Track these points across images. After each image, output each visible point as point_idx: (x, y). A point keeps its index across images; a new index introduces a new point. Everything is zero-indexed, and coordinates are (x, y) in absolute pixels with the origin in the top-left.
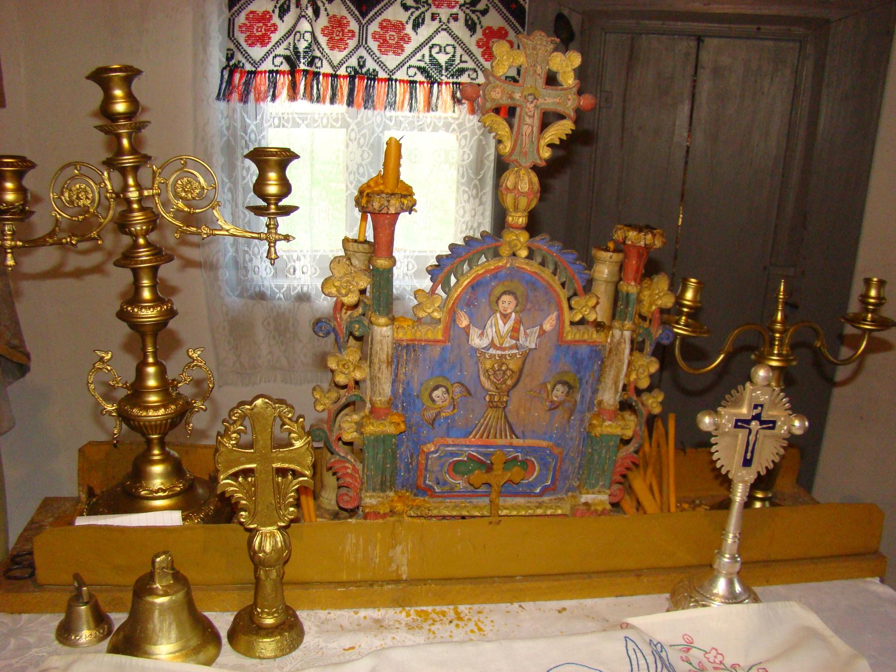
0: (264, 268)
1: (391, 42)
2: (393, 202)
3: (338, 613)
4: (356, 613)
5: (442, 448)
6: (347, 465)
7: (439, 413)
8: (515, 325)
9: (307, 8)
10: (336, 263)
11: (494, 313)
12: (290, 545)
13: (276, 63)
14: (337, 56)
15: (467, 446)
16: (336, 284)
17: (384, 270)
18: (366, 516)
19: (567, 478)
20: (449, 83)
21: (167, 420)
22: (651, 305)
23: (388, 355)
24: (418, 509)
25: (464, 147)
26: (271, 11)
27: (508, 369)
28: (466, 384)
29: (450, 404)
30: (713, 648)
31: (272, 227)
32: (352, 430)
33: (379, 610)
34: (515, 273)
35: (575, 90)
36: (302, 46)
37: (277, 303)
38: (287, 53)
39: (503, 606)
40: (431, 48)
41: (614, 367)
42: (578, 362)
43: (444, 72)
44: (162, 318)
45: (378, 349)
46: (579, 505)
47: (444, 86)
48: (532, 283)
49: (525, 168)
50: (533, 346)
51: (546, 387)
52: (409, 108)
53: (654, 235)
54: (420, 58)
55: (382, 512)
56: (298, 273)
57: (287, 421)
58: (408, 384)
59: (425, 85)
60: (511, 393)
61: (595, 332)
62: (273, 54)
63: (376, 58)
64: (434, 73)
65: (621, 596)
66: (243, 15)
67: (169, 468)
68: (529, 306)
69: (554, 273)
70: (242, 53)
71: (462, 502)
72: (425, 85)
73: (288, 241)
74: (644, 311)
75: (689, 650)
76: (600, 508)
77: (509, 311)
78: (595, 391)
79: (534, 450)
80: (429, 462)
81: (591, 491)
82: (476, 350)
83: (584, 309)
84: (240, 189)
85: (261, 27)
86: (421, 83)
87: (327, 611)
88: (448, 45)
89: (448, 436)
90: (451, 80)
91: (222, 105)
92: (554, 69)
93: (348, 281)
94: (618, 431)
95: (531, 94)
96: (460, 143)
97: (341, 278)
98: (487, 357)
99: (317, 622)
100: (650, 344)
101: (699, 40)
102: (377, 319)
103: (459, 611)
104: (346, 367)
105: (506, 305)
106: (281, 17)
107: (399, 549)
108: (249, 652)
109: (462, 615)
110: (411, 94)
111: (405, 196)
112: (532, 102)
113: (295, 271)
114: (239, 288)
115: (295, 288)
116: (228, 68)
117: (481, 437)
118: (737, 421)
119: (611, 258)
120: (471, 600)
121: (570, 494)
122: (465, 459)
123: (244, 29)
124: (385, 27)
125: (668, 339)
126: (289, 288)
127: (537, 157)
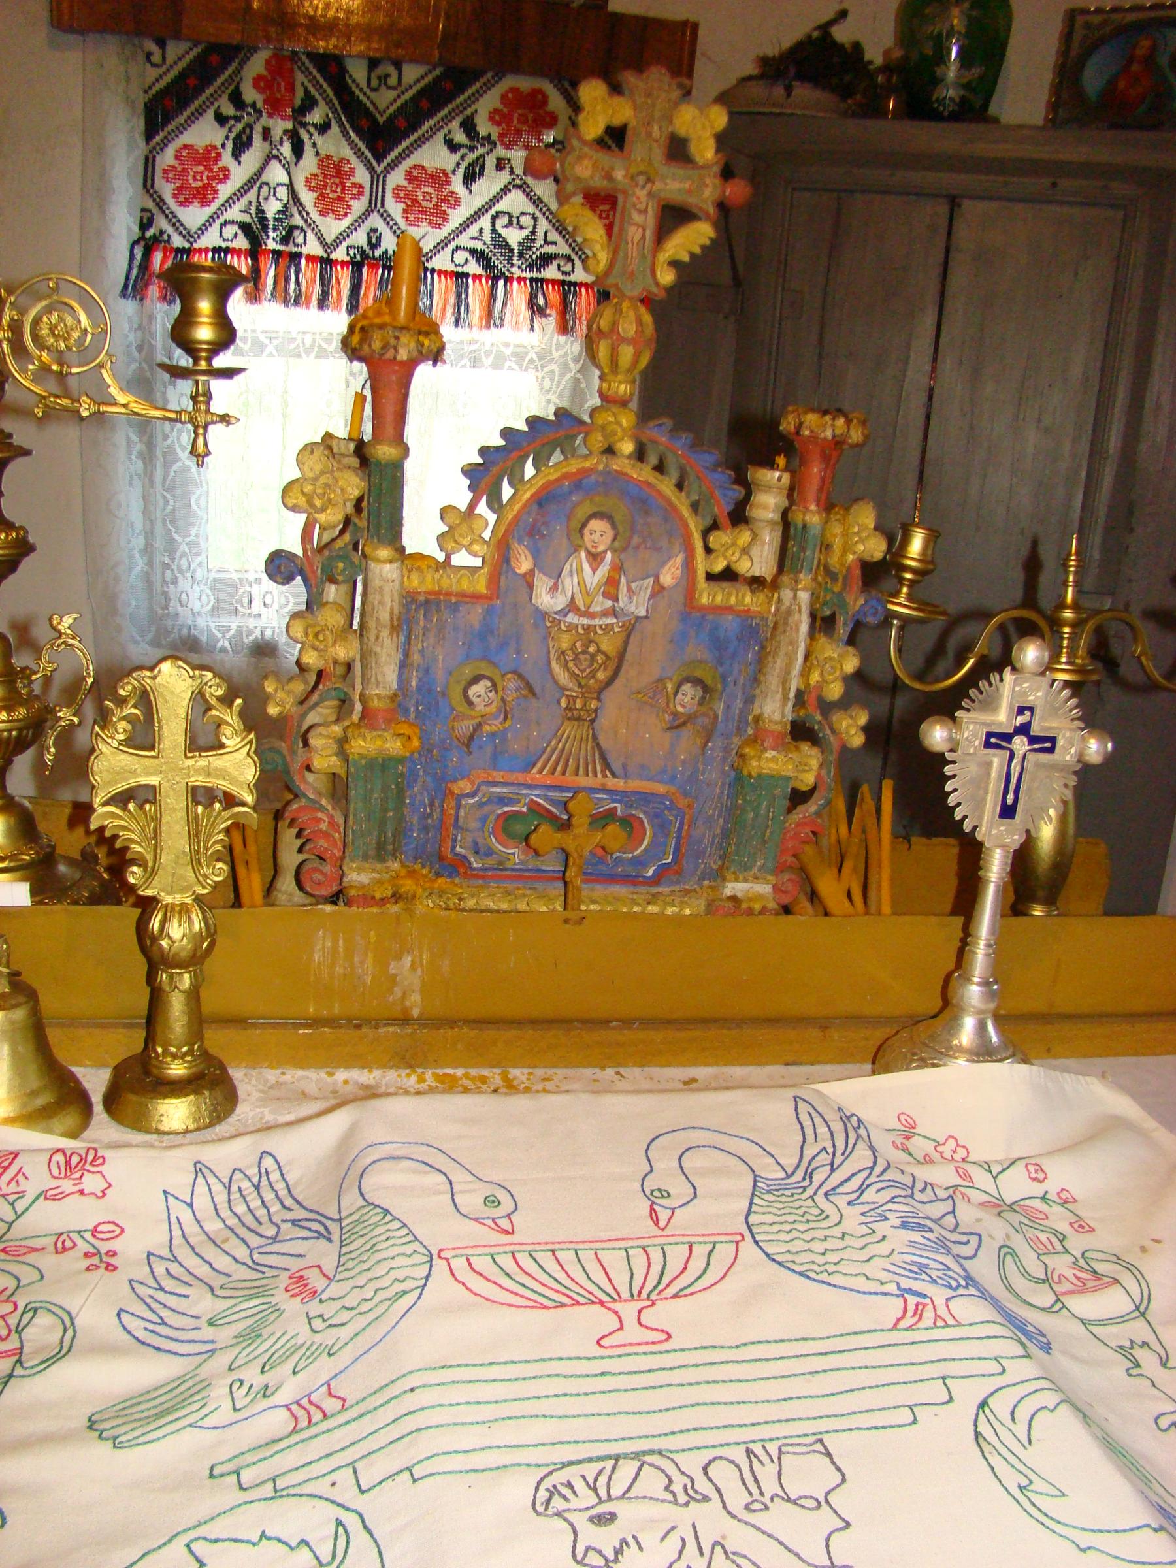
0: (197, 595)
1: (424, 204)
2: (404, 339)
3: (300, 1073)
4: (331, 1074)
5: (483, 788)
6: (320, 815)
7: (480, 725)
8: (612, 573)
9: (281, 144)
10: (307, 453)
11: (576, 550)
12: (215, 932)
13: (225, 235)
14: (332, 227)
15: (530, 787)
16: (306, 490)
17: (387, 465)
18: (348, 903)
19: (700, 854)
20: (524, 279)
21: (10, 731)
22: (845, 552)
23: (392, 614)
24: (441, 896)
25: (549, 391)
26: (219, 144)
27: (599, 651)
28: (526, 675)
29: (499, 710)
30: (952, 1137)
31: (202, 397)
32: (329, 751)
33: (370, 1071)
34: (613, 480)
35: (716, 169)
36: (272, 208)
37: (219, 657)
38: (246, 218)
39: (588, 1072)
40: (494, 218)
41: (782, 653)
42: (718, 645)
43: (515, 260)
44: (7, 552)
45: (376, 602)
46: (721, 900)
47: (515, 284)
48: (643, 501)
49: (631, 298)
50: (643, 613)
51: (666, 688)
52: (453, 319)
53: (849, 422)
54: (476, 234)
55: (378, 896)
56: (257, 607)
57: (213, 702)
58: (427, 670)
59: (484, 280)
60: (606, 695)
61: (749, 593)
62: (222, 220)
63: (398, 232)
64: (499, 262)
65: (794, 1063)
66: (170, 151)
67: (12, 821)
68: (636, 540)
69: (680, 486)
70: (167, 216)
71: (519, 888)
72: (484, 280)
73: (229, 423)
74: (834, 561)
75: (908, 1138)
76: (757, 907)
77: (601, 548)
78: (749, 700)
79: (644, 798)
80: (462, 813)
81: (741, 877)
82: (542, 615)
83: (730, 552)
84: (159, 453)
85: (202, 173)
86: (476, 277)
87: (279, 1071)
88: (523, 214)
89: (495, 768)
90: (528, 275)
91: (129, 307)
92: (682, 132)
93: (327, 486)
94: (788, 770)
95: (641, 173)
96: (541, 384)
97: (316, 479)
98: (563, 628)
99: (261, 1087)
100: (845, 624)
101: (954, 202)
102: (376, 549)
103: (510, 1076)
104: (321, 637)
105: (596, 537)
106: (236, 156)
107: (407, 960)
108: (140, 1121)
109: (515, 1083)
110: (459, 295)
111: (426, 334)
112: (643, 187)
113: (250, 602)
114: (153, 629)
115: (250, 632)
116: (143, 243)
117: (553, 772)
118: (989, 735)
119: (779, 479)
120: (531, 1059)
121: (706, 883)
122: (524, 809)
123: (170, 176)
124: (416, 178)
125: (875, 614)
126: (239, 632)
127: (650, 281)
